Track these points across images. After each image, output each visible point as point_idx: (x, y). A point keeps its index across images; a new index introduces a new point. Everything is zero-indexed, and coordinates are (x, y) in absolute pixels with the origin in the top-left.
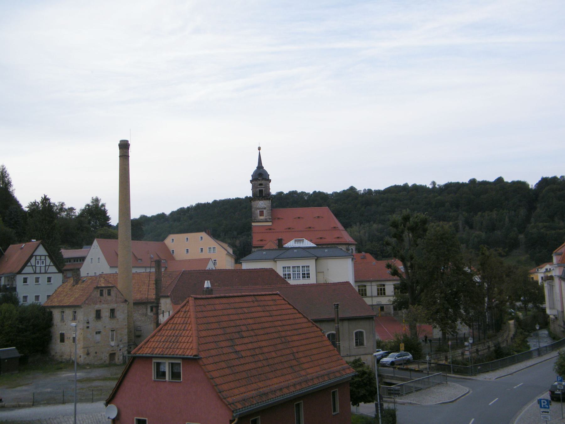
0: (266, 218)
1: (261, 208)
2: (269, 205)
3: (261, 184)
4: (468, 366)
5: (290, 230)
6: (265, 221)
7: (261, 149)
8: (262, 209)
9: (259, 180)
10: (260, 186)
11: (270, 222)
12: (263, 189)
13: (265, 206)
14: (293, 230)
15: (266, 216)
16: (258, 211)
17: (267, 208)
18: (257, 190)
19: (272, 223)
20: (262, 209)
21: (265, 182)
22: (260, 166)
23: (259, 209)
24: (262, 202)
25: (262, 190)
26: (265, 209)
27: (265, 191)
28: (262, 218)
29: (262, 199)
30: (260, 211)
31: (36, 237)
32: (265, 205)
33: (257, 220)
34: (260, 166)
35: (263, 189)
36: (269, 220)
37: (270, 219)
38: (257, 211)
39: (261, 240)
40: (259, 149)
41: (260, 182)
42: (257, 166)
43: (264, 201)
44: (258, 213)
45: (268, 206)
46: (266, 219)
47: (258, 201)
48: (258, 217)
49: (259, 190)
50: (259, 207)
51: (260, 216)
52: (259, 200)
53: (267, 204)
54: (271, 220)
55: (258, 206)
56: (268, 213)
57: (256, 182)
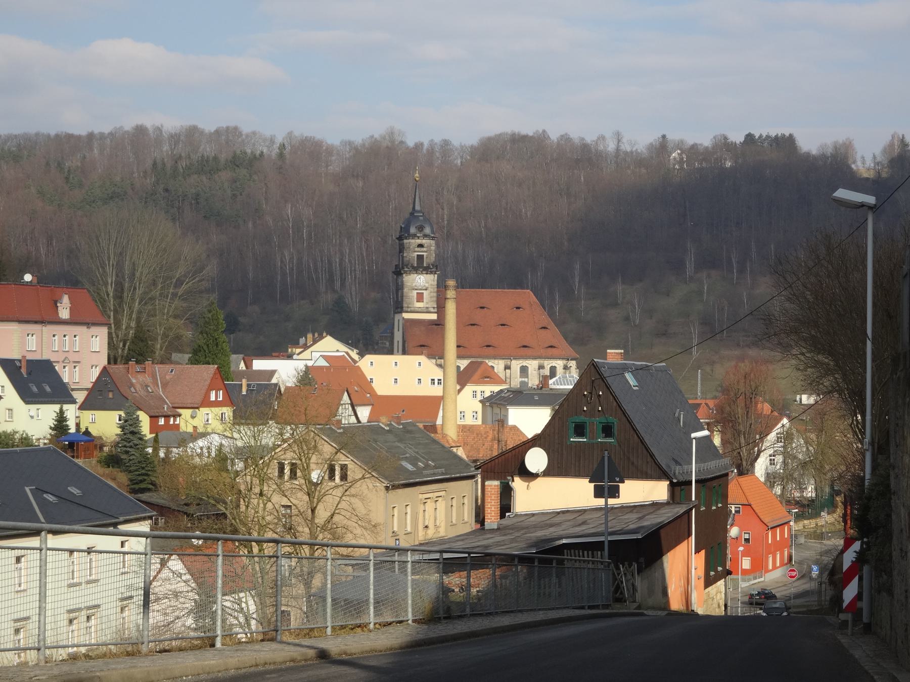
0: (427, 306)
2: (433, 283)
3: (421, 246)
8: (421, 289)
10: (419, 249)
13: (427, 285)
15: (427, 303)
20: (421, 289)
26: (426, 290)
36: (432, 310)
37: (434, 308)
41: (419, 241)
46: (427, 308)
55: (414, 284)
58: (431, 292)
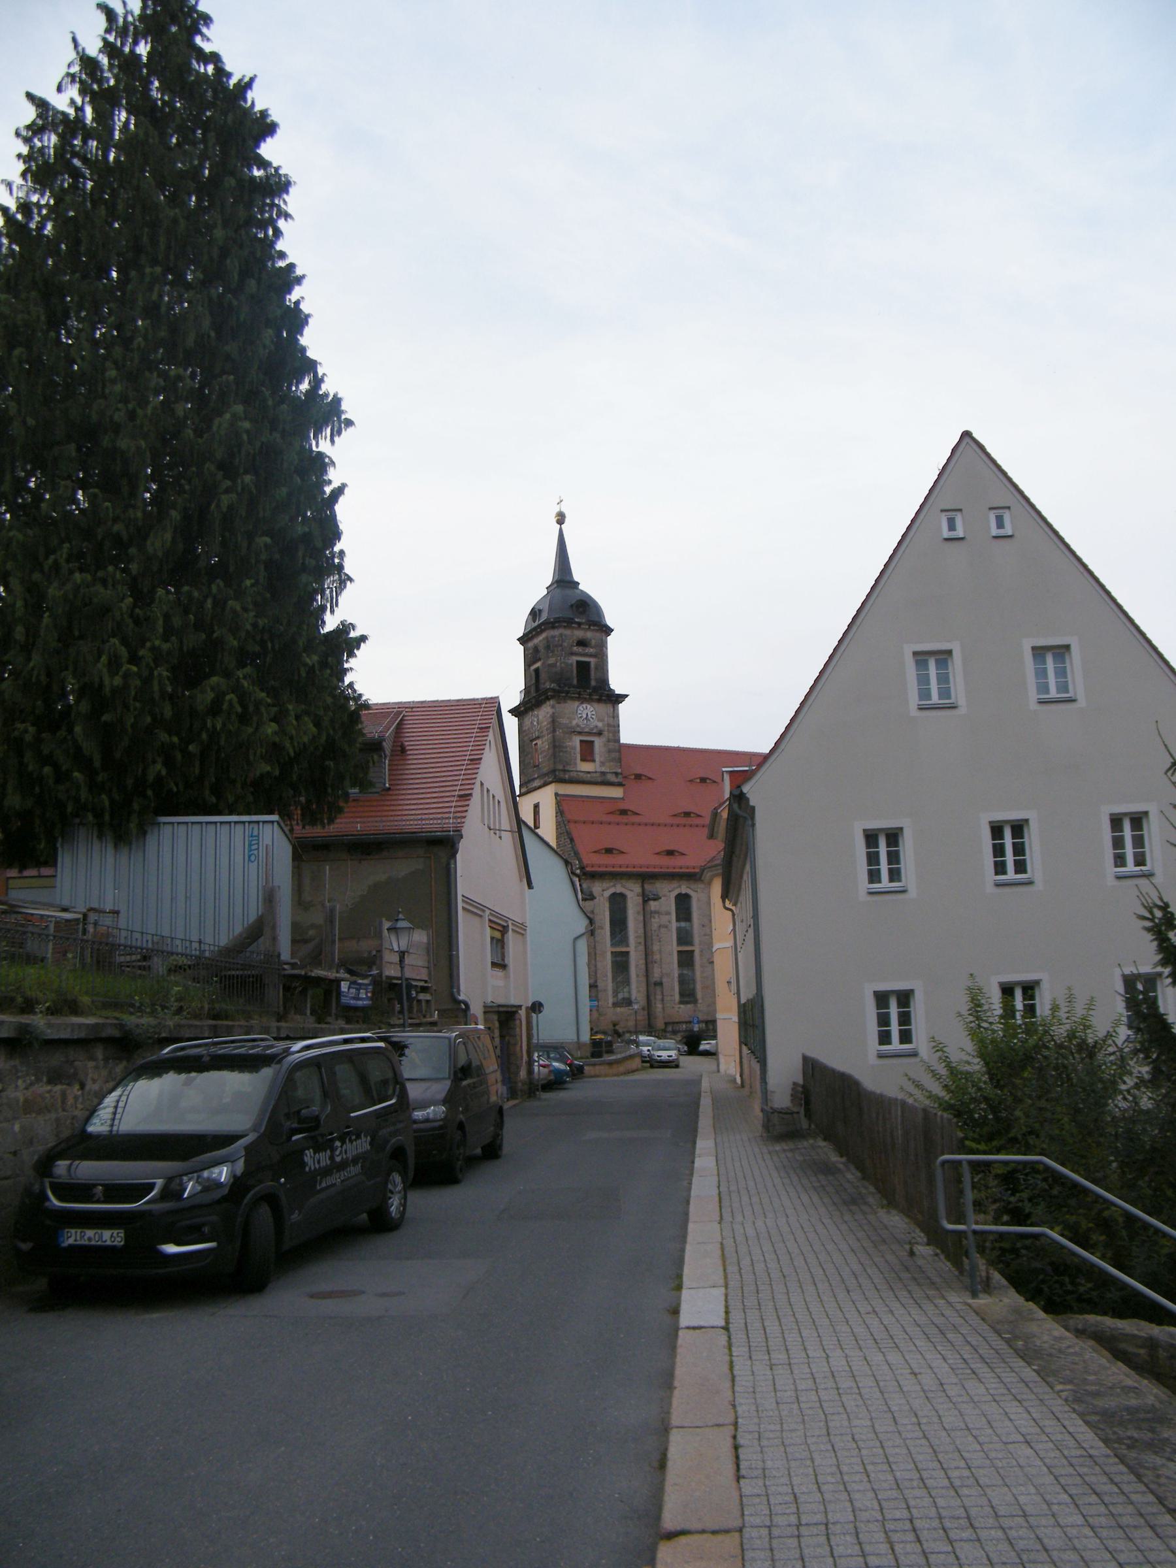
0: (603, 769)
1: (587, 730)
3: (582, 643)
4: (332, 1027)
5: (625, 817)
6: (599, 780)
7: (567, 520)
8: (589, 734)
9: (579, 624)
10: (580, 649)
11: (620, 785)
12: (592, 660)
13: (600, 725)
14: (636, 819)
15: (602, 764)
16: (576, 741)
17: (606, 733)
18: (570, 662)
19: (624, 793)
20: (589, 734)
21: (598, 635)
22: (563, 578)
23: (580, 733)
24: (589, 706)
25: (588, 664)
27: (596, 668)
28: (586, 767)
29: (590, 695)
30: (581, 741)
31: (110, 220)
32: (599, 720)
33: (574, 774)
34: (563, 578)
35: (592, 660)
36: (612, 778)
38: (571, 739)
39: (609, 851)
40: (561, 519)
41: (579, 634)
42: (549, 580)
43: (596, 705)
44: (574, 748)
45: (609, 725)
46: (603, 773)
47: (577, 703)
48: (575, 764)
50: (578, 726)
51: (583, 760)
52: (582, 699)
54: (620, 779)
55: (574, 722)
56: (610, 751)
57: (568, 632)
58: (609, 741)
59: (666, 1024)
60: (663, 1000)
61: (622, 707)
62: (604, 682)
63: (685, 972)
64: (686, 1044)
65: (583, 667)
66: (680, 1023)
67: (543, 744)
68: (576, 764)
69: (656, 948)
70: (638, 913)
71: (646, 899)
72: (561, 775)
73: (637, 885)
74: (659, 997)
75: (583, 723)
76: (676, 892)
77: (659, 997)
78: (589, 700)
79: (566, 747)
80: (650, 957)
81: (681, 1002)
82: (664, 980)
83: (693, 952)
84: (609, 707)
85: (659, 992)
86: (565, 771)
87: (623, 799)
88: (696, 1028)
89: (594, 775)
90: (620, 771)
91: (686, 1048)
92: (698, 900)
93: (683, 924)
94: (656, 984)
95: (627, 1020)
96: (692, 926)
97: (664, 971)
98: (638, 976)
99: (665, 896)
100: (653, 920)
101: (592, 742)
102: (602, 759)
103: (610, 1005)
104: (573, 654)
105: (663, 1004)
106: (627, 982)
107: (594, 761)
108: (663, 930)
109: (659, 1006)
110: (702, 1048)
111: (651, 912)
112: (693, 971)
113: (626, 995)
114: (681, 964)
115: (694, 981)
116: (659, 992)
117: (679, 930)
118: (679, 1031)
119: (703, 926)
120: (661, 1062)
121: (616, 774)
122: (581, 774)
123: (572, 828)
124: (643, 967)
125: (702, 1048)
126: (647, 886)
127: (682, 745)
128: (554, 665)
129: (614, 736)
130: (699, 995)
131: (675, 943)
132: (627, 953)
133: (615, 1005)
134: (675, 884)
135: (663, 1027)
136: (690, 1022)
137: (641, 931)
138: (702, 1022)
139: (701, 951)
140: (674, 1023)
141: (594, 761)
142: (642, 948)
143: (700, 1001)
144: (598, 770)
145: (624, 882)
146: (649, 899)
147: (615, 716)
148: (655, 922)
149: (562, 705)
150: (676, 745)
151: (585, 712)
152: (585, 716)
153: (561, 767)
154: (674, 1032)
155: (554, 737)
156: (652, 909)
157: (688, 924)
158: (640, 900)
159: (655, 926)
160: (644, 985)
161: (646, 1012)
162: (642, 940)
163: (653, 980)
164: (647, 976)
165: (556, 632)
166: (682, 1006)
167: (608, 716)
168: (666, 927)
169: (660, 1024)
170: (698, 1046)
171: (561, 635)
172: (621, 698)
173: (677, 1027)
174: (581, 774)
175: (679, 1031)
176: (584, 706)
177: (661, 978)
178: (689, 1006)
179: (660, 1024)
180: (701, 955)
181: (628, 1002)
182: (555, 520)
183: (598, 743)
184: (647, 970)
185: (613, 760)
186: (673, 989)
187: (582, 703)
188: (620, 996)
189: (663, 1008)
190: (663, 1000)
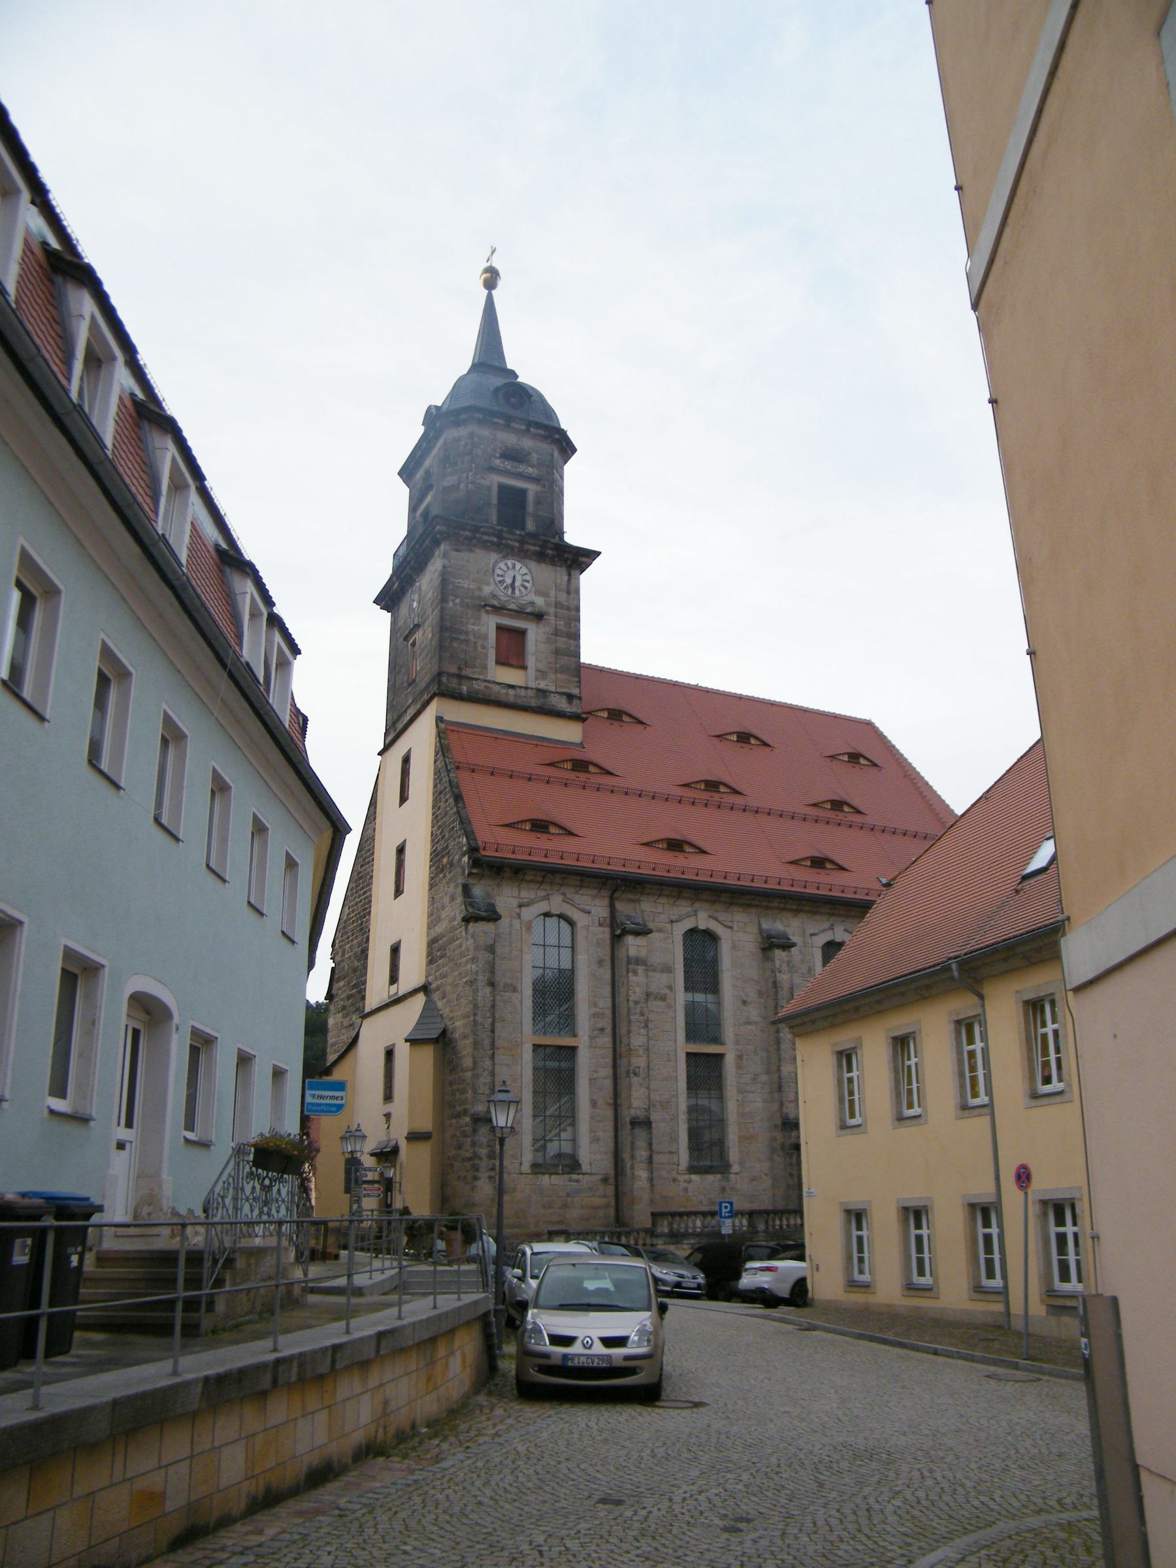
0: (542, 685)
8: (520, 613)
10: (508, 465)
13: (540, 601)
15: (542, 674)
16: (489, 624)
17: (552, 619)
18: (487, 483)
19: (584, 732)
23: (499, 609)
24: (518, 565)
25: (523, 492)
26: (539, 617)
29: (522, 542)
32: (539, 593)
33: (478, 686)
35: (532, 489)
36: (562, 704)
39: (540, 826)
40: (491, 279)
43: (533, 565)
44: (485, 637)
45: (557, 605)
46: (542, 693)
47: (494, 556)
49: (502, 488)
50: (494, 596)
51: (501, 661)
53: (553, 593)
55: (487, 590)
56: (557, 652)
58: (557, 633)
59: (655, 1215)
60: (650, 1160)
61: (588, 580)
62: (553, 525)
63: (701, 1102)
64: (700, 1266)
65: (512, 500)
66: (689, 1214)
67: (425, 636)
68: (485, 667)
69: (637, 1040)
70: (600, 962)
71: (618, 932)
72: (453, 683)
73: (597, 902)
74: (642, 1154)
75: (503, 596)
76: (688, 924)
77: (642, 1154)
78: (522, 554)
79: (466, 633)
80: (623, 1063)
81: (692, 1170)
82: (654, 1117)
83: (720, 1057)
84: (561, 575)
85: (641, 1143)
86: (460, 677)
87: (581, 745)
88: (727, 1228)
89: (523, 693)
90: (575, 691)
91: (701, 1279)
92: (734, 947)
93: (700, 997)
94: (635, 1123)
95: (565, 1206)
96: (719, 1003)
97: (655, 1097)
98: (594, 1103)
99: (660, 930)
100: (632, 978)
101: (522, 633)
102: (542, 666)
103: (526, 1168)
104: (492, 469)
105: (651, 1171)
106: (570, 1116)
107: (523, 667)
108: (654, 1004)
109: (642, 1174)
110: (747, 1281)
111: (629, 961)
112: (721, 1098)
113: (567, 1148)
114: (693, 1085)
115: (721, 1122)
116: (641, 1143)
117: (691, 1009)
118: (686, 1235)
119: (744, 1002)
120: (563, 1369)
121: (570, 697)
122: (496, 688)
123: (466, 782)
124: (608, 1083)
125: (747, 1281)
126: (619, 906)
127: (704, 683)
128: (455, 488)
129: (568, 625)
130: (734, 1155)
131: (681, 1035)
132: (573, 1049)
133: (537, 1168)
134: (684, 908)
135: (647, 1222)
136: (713, 1214)
137: (605, 1003)
138: (741, 1213)
139: (740, 1057)
140: (673, 1215)
141: (523, 667)
142: (607, 1040)
143: (735, 1168)
144: (532, 684)
145: (570, 892)
146: (625, 932)
147: (573, 592)
148: (637, 983)
149: (465, 555)
150: (693, 682)
151: (511, 573)
152: (509, 581)
153: (453, 670)
154: (675, 1237)
155: (442, 610)
156: (632, 952)
157: (710, 997)
158: (605, 933)
159: (637, 993)
160: (609, 1125)
161: (610, 1190)
162: (607, 1023)
163: (627, 1115)
164: (616, 1106)
165: (463, 432)
166: (694, 1177)
167: (558, 589)
168: (663, 998)
169: (641, 1216)
170: (738, 1276)
171: (471, 435)
172: (581, 558)
173: (680, 1225)
174: (496, 688)
175: (686, 1235)
176: (510, 563)
177: (648, 1110)
178: (711, 1177)
179: (641, 1216)
180: (739, 1066)
181: (572, 1165)
182: (481, 282)
183: (535, 634)
184: (616, 1094)
185: (562, 670)
186: (674, 1139)
187: (505, 557)
188: (553, 1148)
189: (651, 1180)
190: (650, 1160)
